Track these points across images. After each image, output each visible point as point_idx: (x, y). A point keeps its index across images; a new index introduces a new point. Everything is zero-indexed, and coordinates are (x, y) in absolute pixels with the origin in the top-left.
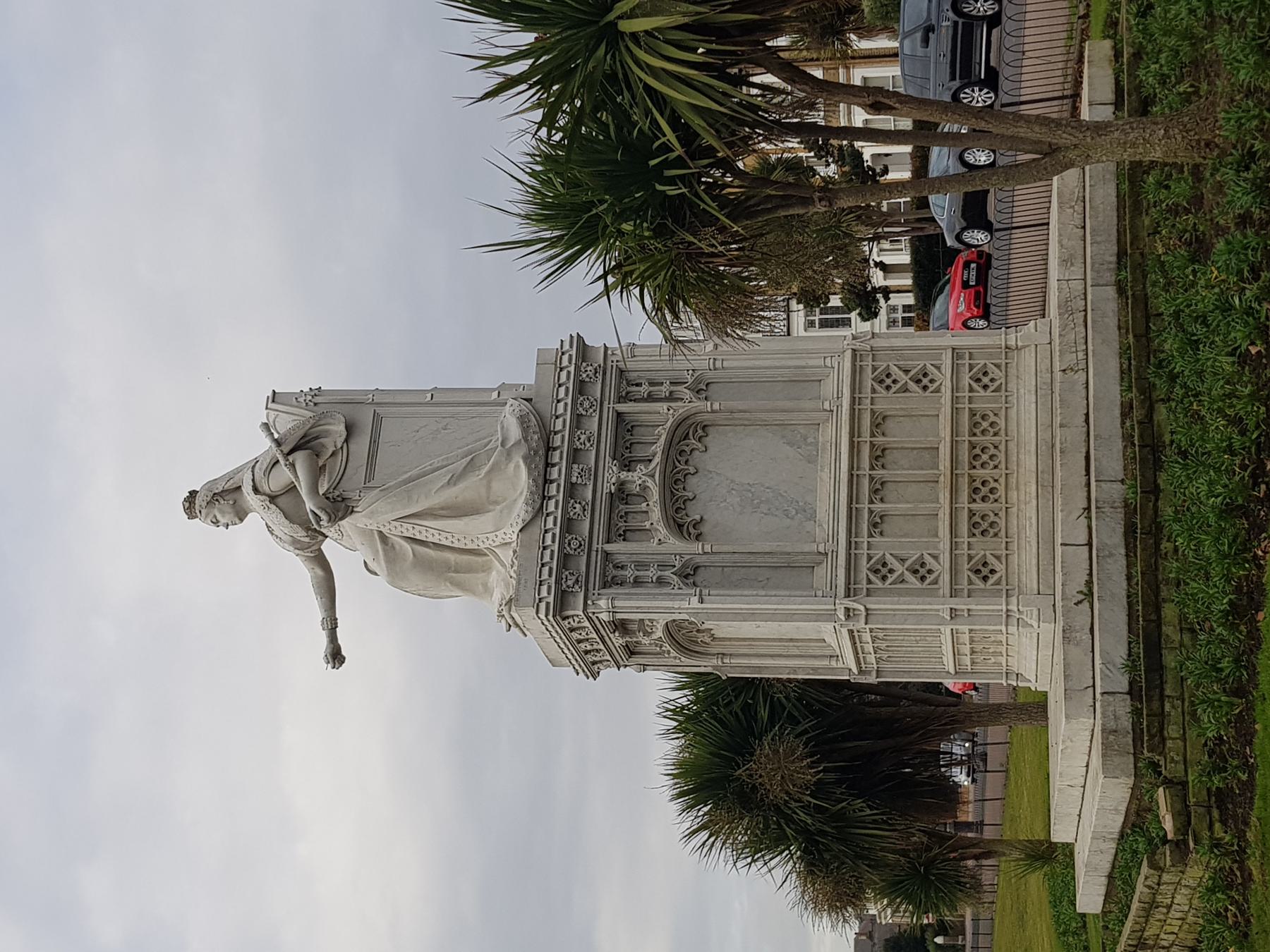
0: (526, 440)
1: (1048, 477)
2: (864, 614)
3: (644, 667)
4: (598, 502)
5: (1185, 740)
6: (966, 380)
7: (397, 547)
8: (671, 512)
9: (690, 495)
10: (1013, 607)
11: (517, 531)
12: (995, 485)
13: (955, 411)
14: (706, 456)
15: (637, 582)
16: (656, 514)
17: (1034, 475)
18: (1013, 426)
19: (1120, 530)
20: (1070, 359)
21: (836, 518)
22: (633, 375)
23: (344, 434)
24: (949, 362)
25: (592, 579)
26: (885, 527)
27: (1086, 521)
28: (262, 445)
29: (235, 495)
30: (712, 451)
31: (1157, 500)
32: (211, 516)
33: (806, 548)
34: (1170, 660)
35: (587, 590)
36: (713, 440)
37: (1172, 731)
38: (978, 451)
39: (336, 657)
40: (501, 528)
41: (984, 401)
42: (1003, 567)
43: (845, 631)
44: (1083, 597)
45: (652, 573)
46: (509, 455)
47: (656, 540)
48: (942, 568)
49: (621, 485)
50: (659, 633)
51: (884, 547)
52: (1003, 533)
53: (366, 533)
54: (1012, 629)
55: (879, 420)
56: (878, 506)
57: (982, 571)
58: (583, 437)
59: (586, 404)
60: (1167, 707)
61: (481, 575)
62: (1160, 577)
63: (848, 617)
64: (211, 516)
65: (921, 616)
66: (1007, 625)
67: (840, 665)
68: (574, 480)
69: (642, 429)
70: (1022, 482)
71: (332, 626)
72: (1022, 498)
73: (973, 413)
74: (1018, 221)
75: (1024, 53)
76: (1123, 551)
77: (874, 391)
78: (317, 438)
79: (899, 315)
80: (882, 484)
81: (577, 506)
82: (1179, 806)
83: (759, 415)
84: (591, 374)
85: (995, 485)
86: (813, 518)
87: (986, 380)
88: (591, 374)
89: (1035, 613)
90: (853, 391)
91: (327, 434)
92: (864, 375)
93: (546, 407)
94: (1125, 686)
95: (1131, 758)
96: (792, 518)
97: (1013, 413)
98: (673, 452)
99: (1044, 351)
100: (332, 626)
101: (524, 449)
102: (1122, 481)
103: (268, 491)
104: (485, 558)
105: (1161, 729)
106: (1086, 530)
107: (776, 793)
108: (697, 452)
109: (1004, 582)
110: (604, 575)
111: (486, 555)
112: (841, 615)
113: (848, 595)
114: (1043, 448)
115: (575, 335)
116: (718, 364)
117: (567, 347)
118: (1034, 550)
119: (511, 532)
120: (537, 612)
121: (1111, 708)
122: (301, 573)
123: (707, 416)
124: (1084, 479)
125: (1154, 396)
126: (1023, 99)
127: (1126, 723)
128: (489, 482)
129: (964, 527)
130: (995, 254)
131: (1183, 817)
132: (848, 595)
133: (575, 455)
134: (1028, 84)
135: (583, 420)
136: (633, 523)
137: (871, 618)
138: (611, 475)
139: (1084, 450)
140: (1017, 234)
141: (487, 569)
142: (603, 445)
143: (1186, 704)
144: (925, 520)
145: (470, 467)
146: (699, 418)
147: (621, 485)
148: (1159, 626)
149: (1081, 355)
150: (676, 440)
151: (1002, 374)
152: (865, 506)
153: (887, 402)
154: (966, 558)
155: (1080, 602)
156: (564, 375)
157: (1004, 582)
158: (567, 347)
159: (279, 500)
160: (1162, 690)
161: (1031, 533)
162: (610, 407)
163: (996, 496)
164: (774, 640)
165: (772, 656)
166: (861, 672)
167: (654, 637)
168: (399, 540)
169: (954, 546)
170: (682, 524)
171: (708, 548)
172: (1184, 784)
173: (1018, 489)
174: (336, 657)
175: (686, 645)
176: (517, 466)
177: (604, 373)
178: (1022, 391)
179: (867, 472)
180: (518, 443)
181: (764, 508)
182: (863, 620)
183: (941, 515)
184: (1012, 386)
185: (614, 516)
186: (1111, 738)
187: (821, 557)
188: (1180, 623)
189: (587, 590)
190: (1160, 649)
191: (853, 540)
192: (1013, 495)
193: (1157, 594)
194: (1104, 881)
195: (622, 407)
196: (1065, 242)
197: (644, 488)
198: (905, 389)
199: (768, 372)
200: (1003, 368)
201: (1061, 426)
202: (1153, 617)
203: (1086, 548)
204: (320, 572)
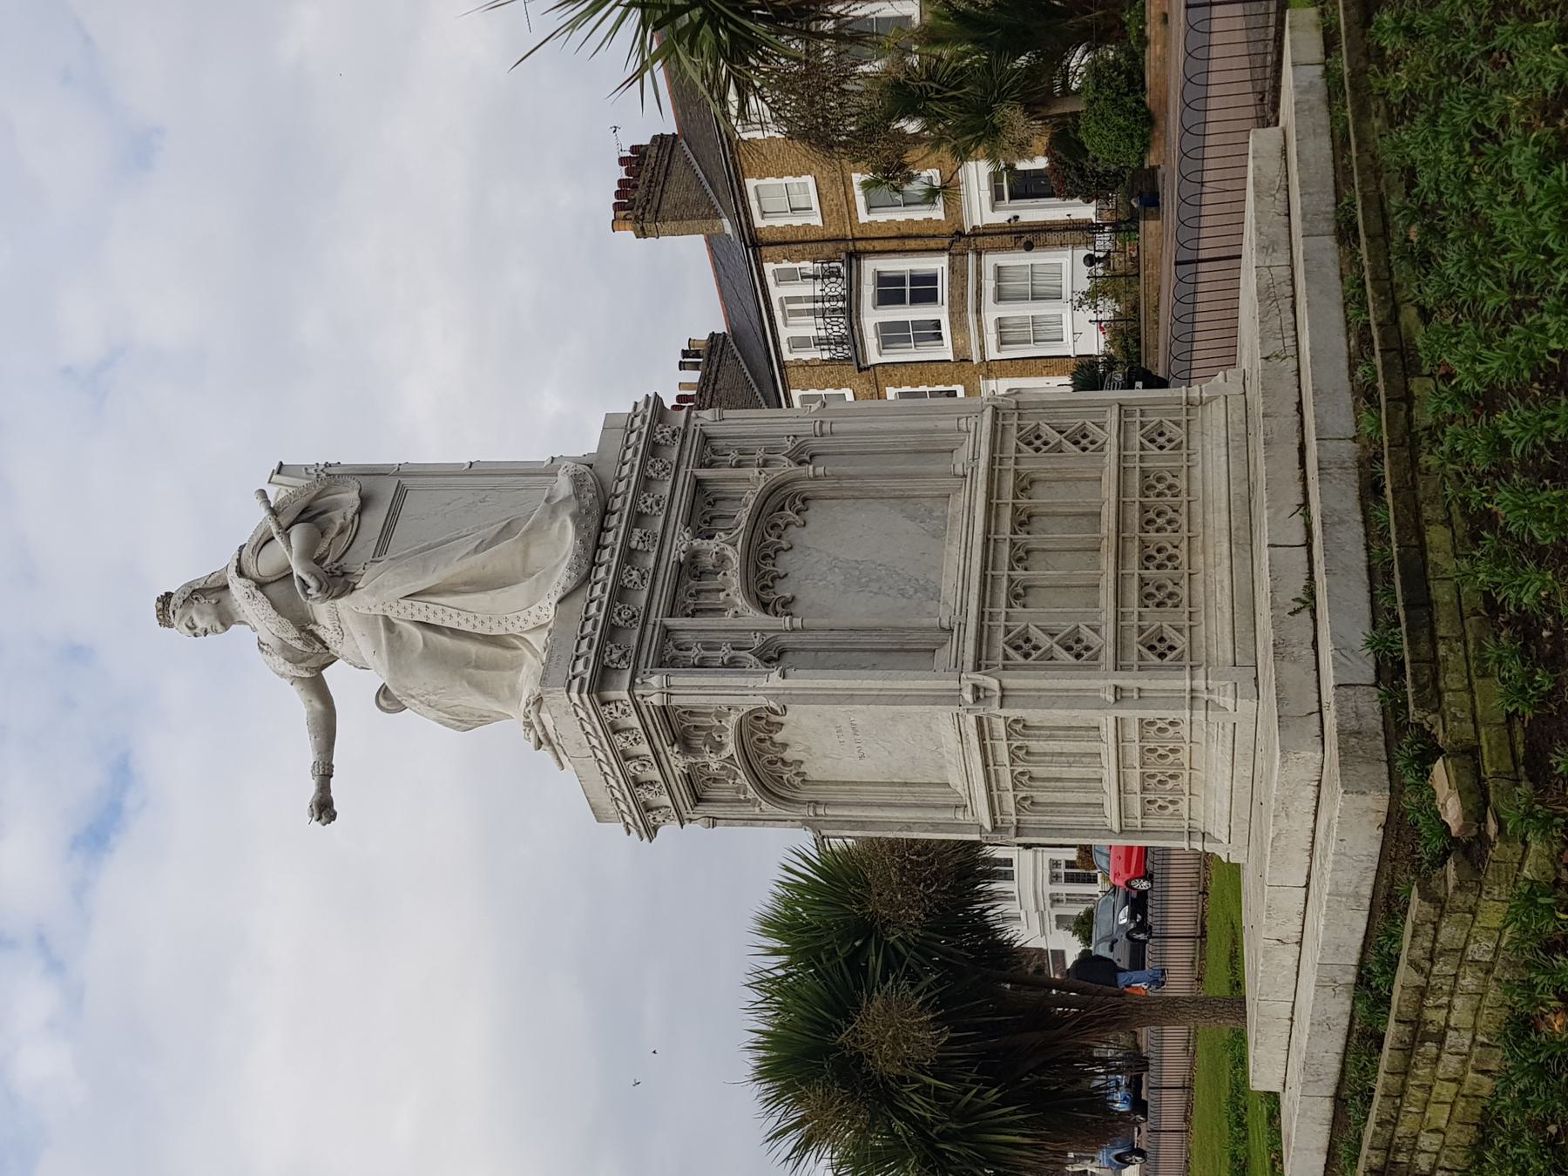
0: (577, 496)
1: (1244, 534)
2: (999, 694)
3: (714, 821)
4: (662, 572)
5: (1472, 692)
6: (1136, 437)
7: (405, 635)
8: (754, 588)
9: (781, 572)
10: (1200, 683)
11: (554, 600)
12: (1175, 551)
13: (1122, 471)
14: (804, 532)
15: (702, 664)
16: (735, 582)
17: (1226, 533)
18: (1197, 486)
19: (1353, 493)
20: (1275, 346)
21: (966, 587)
22: (720, 444)
23: (357, 503)
24: (1115, 418)
25: (644, 656)
26: (1030, 600)
27: (1302, 519)
28: (258, 516)
29: (222, 595)
30: (810, 526)
31: (1410, 409)
32: (186, 618)
33: (926, 622)
34: (1442, 593)
35: (636, 667)
36: (814, 513)
37: (1452, 680)
38: (1152, 515)
39: (324, 809)
40: (533, 607)
41: (1159, 461)
42: (1186, 640)
43: (971, 719)
44: (1298, 605)
45: (725, 653)
46: (554, 512)
47: (732, 612)
48: (1105, 641)
49: (694, 555)
50: (731, 748)
51: (1026, 619)
52: (1185, 601)
53: (368, 621)
54: (1200, 715)
55: (1025, 483)
56: (1023, 502)
57: (1159, 647)
58: (650, 501)
59: (658, 466)
60: (1442, 650)
61: (508, 674)
62: (1421, 496)
63: (977, 699)
64: (186, 618)
65: (1075, 699)
66: (1191, 709)
67: (969, 818)
68: (633, 544)
69: (726, 503)
70: (1210, 543)
71: (325, 775)
72: (1210, 560)
73: (1145, 474)
74: (1172, 932)
75: (1202, 184)
76: (1359, 517)
77: (1019, 451)
78: (325, 512)
79: (1062, 870)
80: (1028, 552)
81: (635, 573)
82: (1468, 781)
83: (878, 484)
84: (668, 436)
85: (1175, 551)
86: (936, 596)
87: (1161, 440)
88: (668, 436)
89: (1230, 687)
90: (993, 450)
91: (337, 505)
92: (1008, 436)
93: (608, 472)
94: (1369, 675)
95: (1385, 768)
96: (910, 598)
97: (1197, 472)
98: (762, 523)
99: (1236, 405)
100: (325, 775)
101: (573, 506)
102: (1354, 439)
103: (255, 575)
104: (514, 653)
105: (1435, 679)
106: (1303, 529)
107: (885, 1065)
108: (792, 529)
109: (1187, 657)
110: (661, 652)
111: (516, 648)
112: (968, 697)
113: (977, 668)
114: (1237, 504)
115: (651, 395)
116: (826, 428)
117: (641, 407)
118: (1228, 615)
119: (546, 609)
120: (568, 691)
121: (1351, 704)
122: (297, 707)
123: (809, 485)
124: (1298, 473)
125: (1399, 296)
126: (1203, 255)
127: (1374, 721)
128: (527, 546)
129: (1133, 596)
130: (1150, 1103)
131: (1477, 800)
132: (977, 668)
133: (638, 518)
134: (1204, 335)
135: (653, 484)
136: (705, 601)
137: (1007, 701)
138: (681, 542)
139: (1297, 441)
140: (1171, 942)
141: (516, 666)
142: (674, 511)
143: (1471, 646)
144: (1084, 588)
145: (507, 531)
146: (798, 487)
147: (694, 555)
148: (1423, 554)
149: (1289, 342)
150: (767, 511)
151: (1182, 432)
152: (1003, 572)
153: (1032, 463)
154: (1135, 630)
155: (1296, 611)
156: (633, 437)
157: (1187, 657)
158: (641, 407)
159: (269, 589)
160: (1433, 631)
161: (1223, 599)
162: (688, 471)
163: (1176, 563)
164: (883, 784)
165: (880, 806)
166: (995, 828)
167: (725, 754)
168: (407, 625)
169: (1119, 616)
170: (764, 590)
171: (797, 622)
172: (1473, 752)
173: (1204, 552)
174: (324, 809)
175: (768, 783)
176: (563, 527)
177: (685, 437)
178: (1209, 447)
179: (1010, 501)
180: (566, 499)
181: (874, 587)
182: (996, 702)
183: (1103, 582)
184: (1196, 443)
185: (682, 591)
186: (1353, 741)
187: (944, 635)
188: (1454, 547)
189: (636, 667)
190: (1427, 580)
191: (987, 610)
192: (1198, 560)
193: (1418, 514)
194: (1327, 1105)
195: (703, 473)
196: (1264, 229)
197: (722, 559)
198: (1058, 449)
199: (890, 439)
200: (1184, 425)
201: (1265, 415)
202: (1414, 542)
203: (1304, 550)
204: (318, 706)
